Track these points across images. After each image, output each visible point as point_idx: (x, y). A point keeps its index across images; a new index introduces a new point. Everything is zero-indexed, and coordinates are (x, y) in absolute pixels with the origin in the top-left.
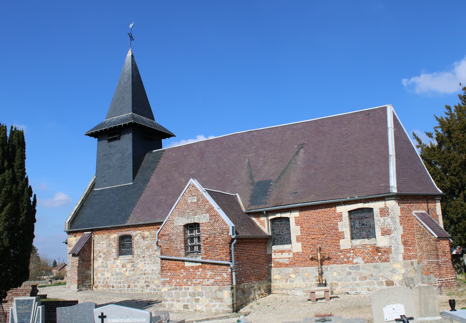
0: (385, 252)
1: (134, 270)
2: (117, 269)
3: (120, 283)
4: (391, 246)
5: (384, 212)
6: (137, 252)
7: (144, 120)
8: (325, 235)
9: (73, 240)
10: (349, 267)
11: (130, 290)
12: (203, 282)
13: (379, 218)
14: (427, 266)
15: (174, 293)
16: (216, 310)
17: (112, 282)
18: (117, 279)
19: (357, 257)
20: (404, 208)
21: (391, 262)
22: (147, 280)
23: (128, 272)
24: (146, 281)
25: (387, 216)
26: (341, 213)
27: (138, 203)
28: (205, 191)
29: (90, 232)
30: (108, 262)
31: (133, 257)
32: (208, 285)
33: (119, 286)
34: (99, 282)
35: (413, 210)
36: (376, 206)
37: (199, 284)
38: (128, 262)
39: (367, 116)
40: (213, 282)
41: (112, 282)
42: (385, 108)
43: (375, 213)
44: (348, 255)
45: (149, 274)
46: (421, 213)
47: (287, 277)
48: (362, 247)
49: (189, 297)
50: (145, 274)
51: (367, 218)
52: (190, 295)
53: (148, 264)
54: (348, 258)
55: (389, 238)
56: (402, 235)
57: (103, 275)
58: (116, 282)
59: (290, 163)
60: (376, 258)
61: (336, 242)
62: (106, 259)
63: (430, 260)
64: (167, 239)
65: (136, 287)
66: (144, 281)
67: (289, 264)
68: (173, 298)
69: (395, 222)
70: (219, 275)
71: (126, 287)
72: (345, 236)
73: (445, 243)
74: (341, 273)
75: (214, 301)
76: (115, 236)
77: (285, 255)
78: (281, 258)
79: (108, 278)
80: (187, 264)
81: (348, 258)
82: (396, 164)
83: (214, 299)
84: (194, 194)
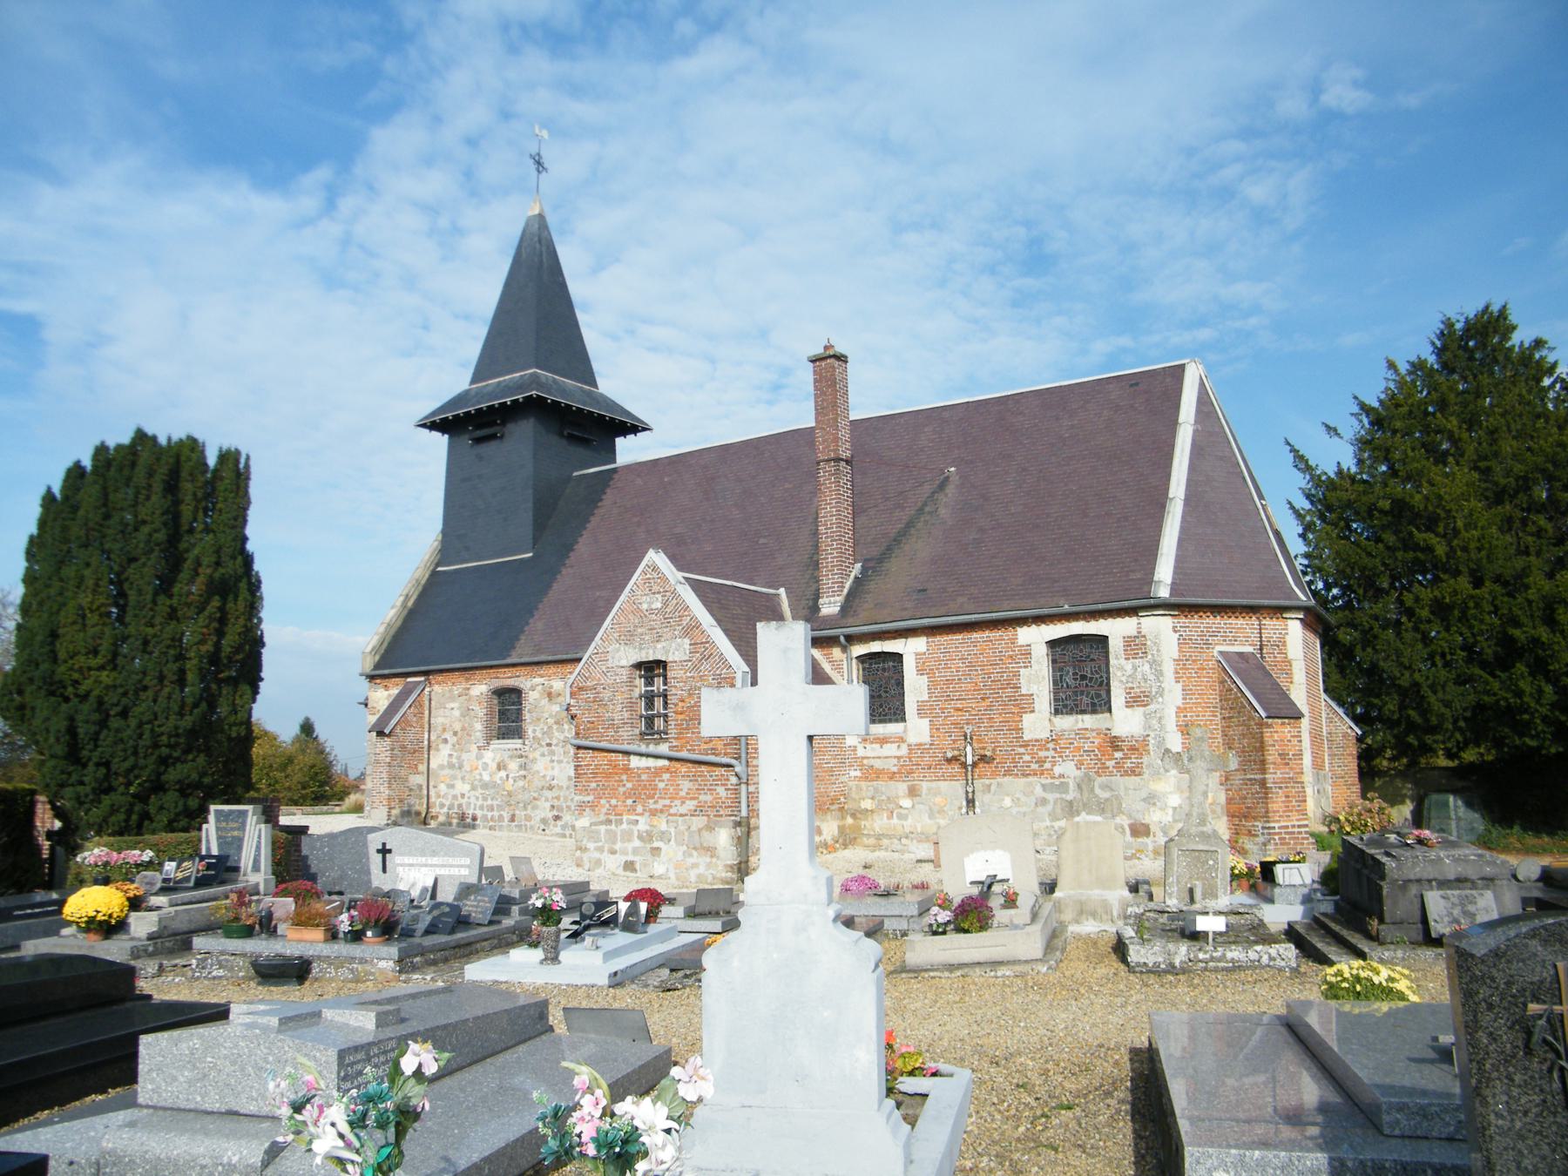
0: (1133, 749)
1: (525, 777)
2: (484, 773)
3: (492, 810)
4: (1148, 736)
5: (1135, 646)
6: (534, 731)
7: (562, 388)
8: (987, 702)
9: (382, 697)
10: (1043, 785)
11: (516, 826)
12: (671, 806)
13: (1123, 661)
14: (1241, 789)
15: (603, 831)
16: (699, 876)
17: (472, 806)
18: (485, 799)
19: (1063, 761)
20: (1191, 639)
21: (1146, 776)
22: (556, 803)
23: (511, 781)
24: (553, 807)
25: (1142, 658)
26: (1029, 645)
27: (540, 606)
28: (683, 581)
29: (422, 679)
30: (465, 756)
31: (524, 744)
32: (681, 815)
33: (489, 817)
34: (442, 806)
35: (1216, 644)
36: (1115, 629)
37: (662, 811)
38: (511, 757)
39: (1132, 389)
40: (693, 808)
41: (472, 806)
42: (1182, 368)
43: (1111, 649)
44: (1042, 754)
45: (561, 788)
46: (1241, 655)
47: (891, 806)
48: (1076, 734)
49: (637, 843)
50: (551, 788)
51: (1092, 660)
52: (640, 837)
53: (560, 762)
54: (1041, 762)
55: (1145, 715)
56: (1179, 708)
57: (452, 786)
58: (482, 808)
59: (921, 510)
60: (1111, 764)
61: (1013, 721)
62: (460, 746)
63: (1248, 776)
64: (591, 699)
65: (530, 821)
66: (548, 805)
67: (898, 773)
68: (600, 844)
69: (1159, 674)
70: (709, 790)
71: (506, 820)
72: (1037, 706)
73: (1290, 732)
74: (1022, 799)
75: (695, 853)
76: (480, 688)
77: (890, 750)
78: (879, 758)
79: (463, 796)
80: (635, 762)
81: (1041, 762)
82: (1182, 522)
83: (695, 848)
84: (656, 588)
